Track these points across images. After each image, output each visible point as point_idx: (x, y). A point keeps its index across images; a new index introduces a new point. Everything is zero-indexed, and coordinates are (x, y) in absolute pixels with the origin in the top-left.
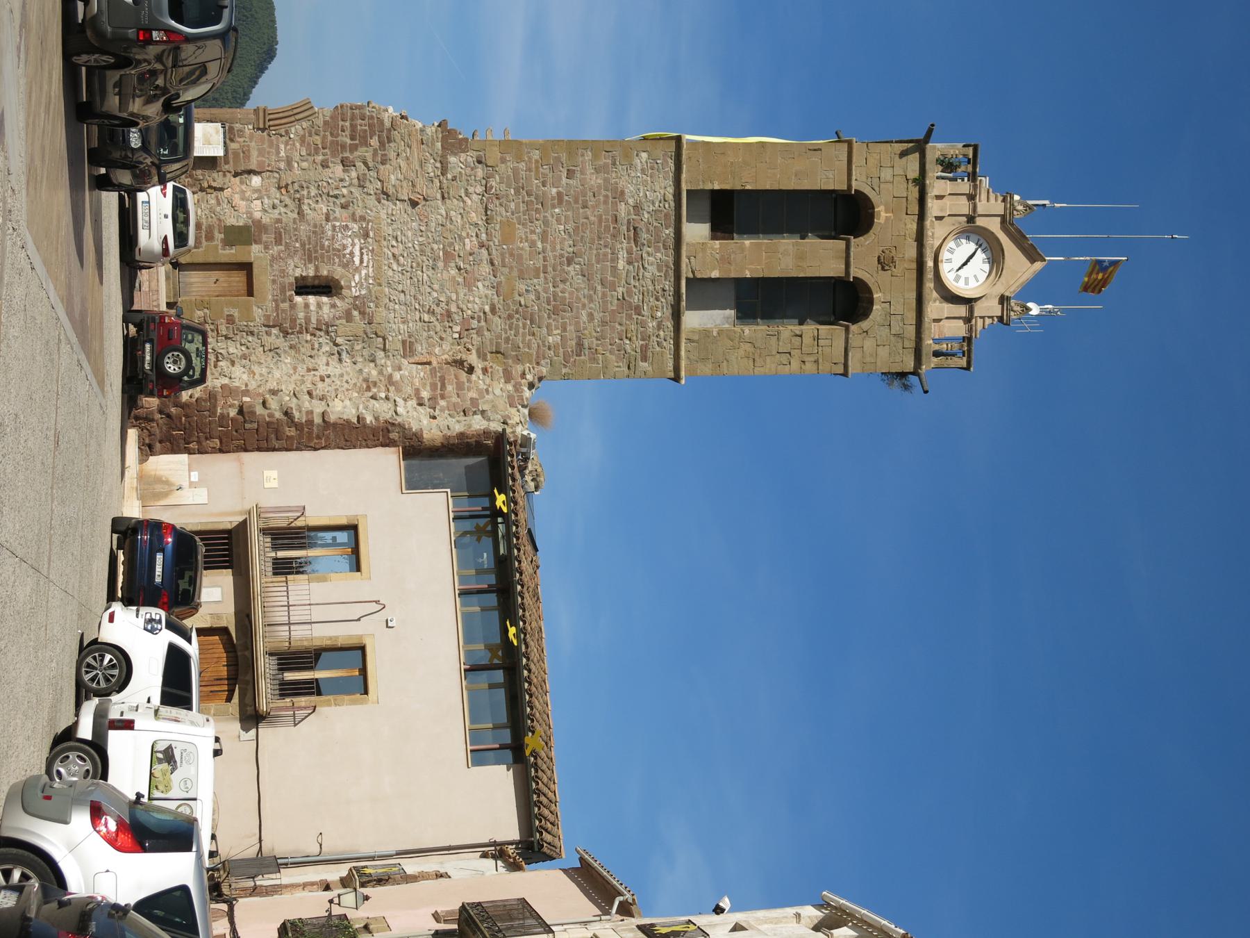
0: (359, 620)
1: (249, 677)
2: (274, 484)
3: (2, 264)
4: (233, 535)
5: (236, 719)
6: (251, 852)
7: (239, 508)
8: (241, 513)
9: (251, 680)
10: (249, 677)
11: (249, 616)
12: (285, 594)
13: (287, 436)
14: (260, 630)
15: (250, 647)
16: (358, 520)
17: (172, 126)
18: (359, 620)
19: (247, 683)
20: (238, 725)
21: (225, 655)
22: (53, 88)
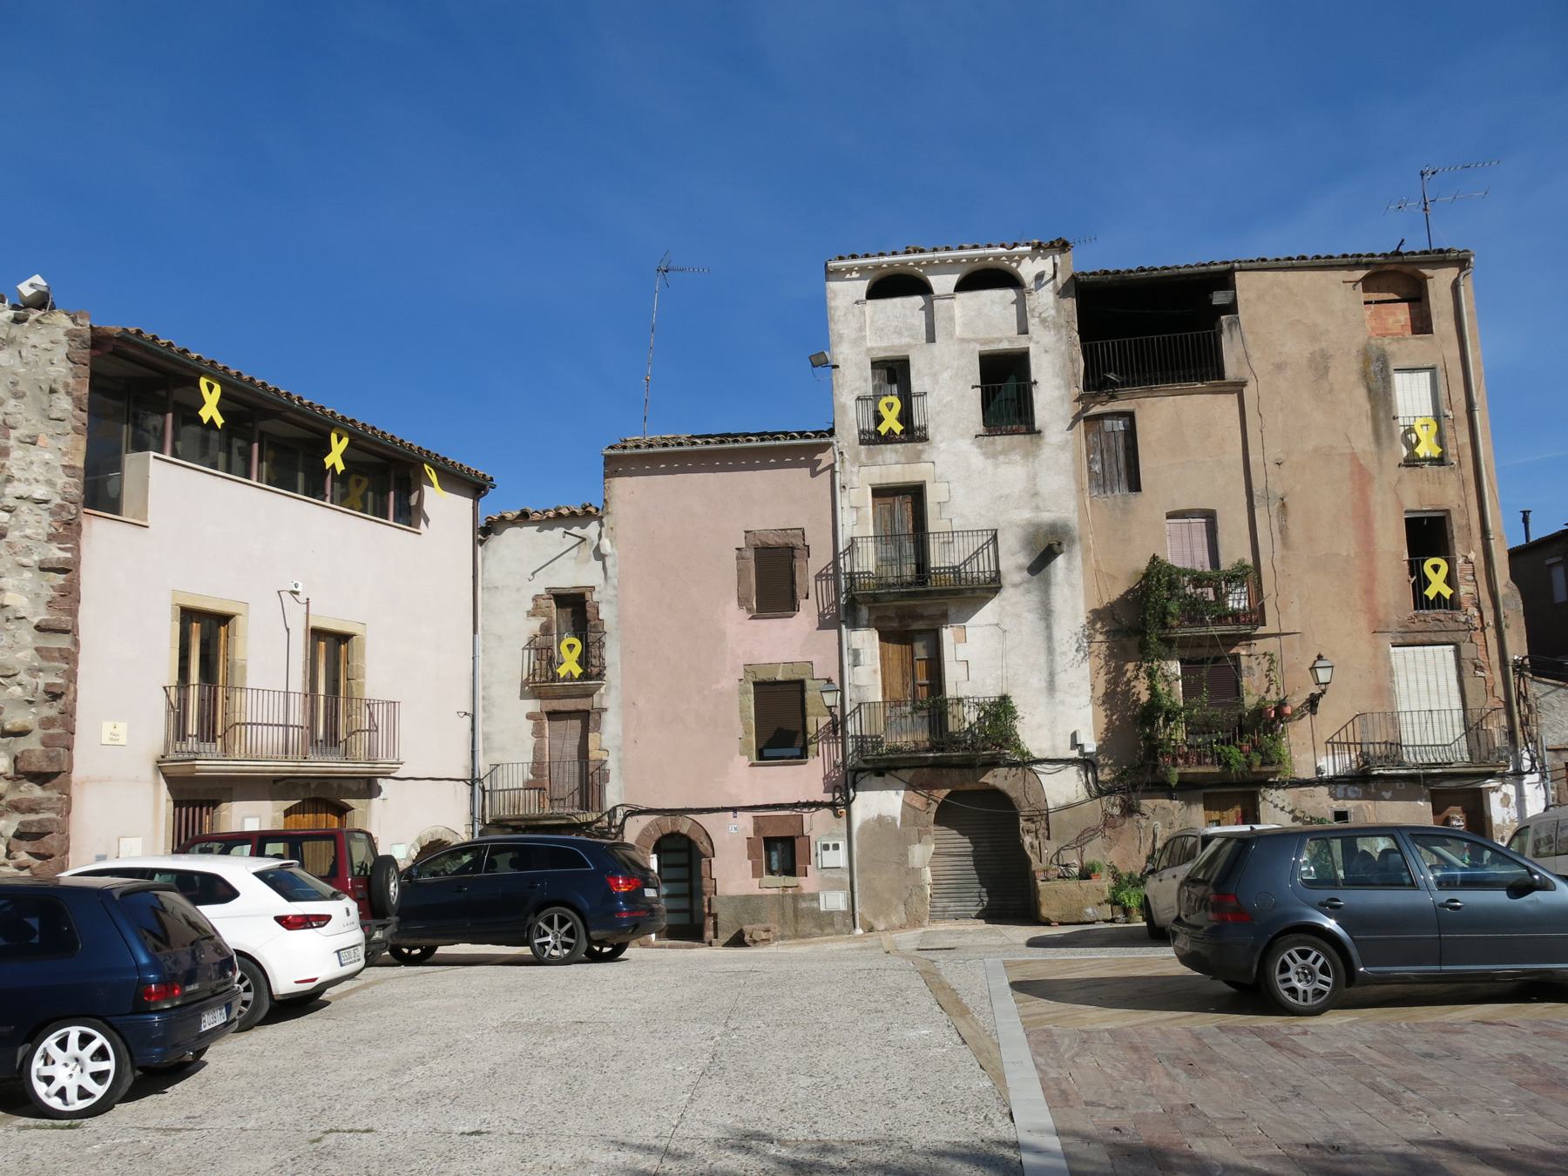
0: (288, 630)
1: (335, 784)
2: (122, 728)
3: (884, 1168)
4: (185, 797)
5: (369, 803)
6: (464, 789)
7: (149, 788)
8: (157, 785)
9: (337, 781)
10: (335, 784)
11: (276, 780)
12: (254, 727)
13: (528, 786)
14: (286, 766)
15: (308, 780)
16: (177, 605)
17: (1209, 974)
18: (288, 630)
19: (340, 786)
20: (375, 801)
21: (293, 816)
22: (1417, 987)
